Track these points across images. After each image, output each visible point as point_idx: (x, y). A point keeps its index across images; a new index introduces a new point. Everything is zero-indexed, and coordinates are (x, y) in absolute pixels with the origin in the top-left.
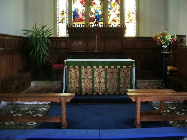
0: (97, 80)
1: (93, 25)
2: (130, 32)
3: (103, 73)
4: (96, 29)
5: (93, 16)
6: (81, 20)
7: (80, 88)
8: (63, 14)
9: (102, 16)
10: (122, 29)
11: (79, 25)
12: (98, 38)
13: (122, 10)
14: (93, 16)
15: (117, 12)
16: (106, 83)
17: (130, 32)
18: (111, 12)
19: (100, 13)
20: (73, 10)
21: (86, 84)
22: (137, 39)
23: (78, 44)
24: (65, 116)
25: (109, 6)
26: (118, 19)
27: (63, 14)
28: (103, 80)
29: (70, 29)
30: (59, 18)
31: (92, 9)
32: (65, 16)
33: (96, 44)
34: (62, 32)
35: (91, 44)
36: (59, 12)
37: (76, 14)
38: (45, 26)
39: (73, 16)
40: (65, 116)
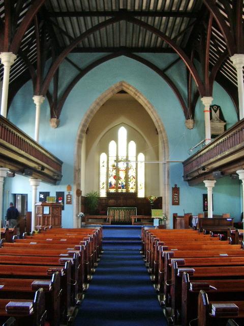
0: (121, 216)
1: (120, 191)
2: (141, 194)
3: (124, 213)
4: (122, 193)
5: (120, 185)
6: (113, 188)
7: (114, 219)
8: (103, 184)
9: (125, 185)
10: (136, 194)
11: (112, 191)
12: (105, 217)
13: (136, 182)
14: (120, 185)
15: (134, 183)
16: (125, 217)
17: (141, 194)
18: (130, 183)
19: (124, 184)
20: (109, 182)
21: (116, 217)
22: (145, 199)
23: (111, 201)
24: (117, 190)
25: (129, 180)
26: (135, 187)
27: (103, 184)
28: (123, 216)
29: (108, 193)
30: (101, 186)
31: (120, 182)
32: (105, 185)
33: (121, 201)
34: (103, 194)
35: (119, 201)
36: (101, 183)
37: (111, 184)
38: (9, 110)
39: (110, 185)
40: (117, 190)
